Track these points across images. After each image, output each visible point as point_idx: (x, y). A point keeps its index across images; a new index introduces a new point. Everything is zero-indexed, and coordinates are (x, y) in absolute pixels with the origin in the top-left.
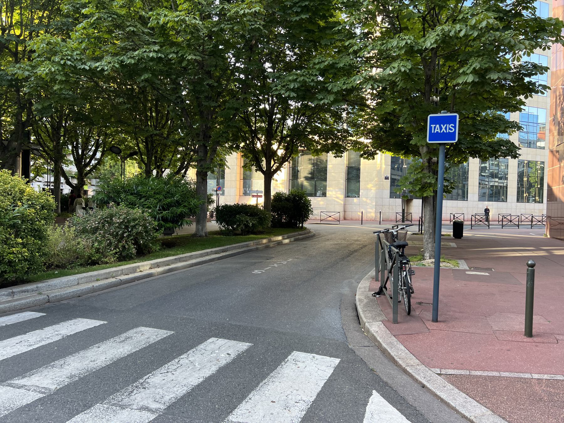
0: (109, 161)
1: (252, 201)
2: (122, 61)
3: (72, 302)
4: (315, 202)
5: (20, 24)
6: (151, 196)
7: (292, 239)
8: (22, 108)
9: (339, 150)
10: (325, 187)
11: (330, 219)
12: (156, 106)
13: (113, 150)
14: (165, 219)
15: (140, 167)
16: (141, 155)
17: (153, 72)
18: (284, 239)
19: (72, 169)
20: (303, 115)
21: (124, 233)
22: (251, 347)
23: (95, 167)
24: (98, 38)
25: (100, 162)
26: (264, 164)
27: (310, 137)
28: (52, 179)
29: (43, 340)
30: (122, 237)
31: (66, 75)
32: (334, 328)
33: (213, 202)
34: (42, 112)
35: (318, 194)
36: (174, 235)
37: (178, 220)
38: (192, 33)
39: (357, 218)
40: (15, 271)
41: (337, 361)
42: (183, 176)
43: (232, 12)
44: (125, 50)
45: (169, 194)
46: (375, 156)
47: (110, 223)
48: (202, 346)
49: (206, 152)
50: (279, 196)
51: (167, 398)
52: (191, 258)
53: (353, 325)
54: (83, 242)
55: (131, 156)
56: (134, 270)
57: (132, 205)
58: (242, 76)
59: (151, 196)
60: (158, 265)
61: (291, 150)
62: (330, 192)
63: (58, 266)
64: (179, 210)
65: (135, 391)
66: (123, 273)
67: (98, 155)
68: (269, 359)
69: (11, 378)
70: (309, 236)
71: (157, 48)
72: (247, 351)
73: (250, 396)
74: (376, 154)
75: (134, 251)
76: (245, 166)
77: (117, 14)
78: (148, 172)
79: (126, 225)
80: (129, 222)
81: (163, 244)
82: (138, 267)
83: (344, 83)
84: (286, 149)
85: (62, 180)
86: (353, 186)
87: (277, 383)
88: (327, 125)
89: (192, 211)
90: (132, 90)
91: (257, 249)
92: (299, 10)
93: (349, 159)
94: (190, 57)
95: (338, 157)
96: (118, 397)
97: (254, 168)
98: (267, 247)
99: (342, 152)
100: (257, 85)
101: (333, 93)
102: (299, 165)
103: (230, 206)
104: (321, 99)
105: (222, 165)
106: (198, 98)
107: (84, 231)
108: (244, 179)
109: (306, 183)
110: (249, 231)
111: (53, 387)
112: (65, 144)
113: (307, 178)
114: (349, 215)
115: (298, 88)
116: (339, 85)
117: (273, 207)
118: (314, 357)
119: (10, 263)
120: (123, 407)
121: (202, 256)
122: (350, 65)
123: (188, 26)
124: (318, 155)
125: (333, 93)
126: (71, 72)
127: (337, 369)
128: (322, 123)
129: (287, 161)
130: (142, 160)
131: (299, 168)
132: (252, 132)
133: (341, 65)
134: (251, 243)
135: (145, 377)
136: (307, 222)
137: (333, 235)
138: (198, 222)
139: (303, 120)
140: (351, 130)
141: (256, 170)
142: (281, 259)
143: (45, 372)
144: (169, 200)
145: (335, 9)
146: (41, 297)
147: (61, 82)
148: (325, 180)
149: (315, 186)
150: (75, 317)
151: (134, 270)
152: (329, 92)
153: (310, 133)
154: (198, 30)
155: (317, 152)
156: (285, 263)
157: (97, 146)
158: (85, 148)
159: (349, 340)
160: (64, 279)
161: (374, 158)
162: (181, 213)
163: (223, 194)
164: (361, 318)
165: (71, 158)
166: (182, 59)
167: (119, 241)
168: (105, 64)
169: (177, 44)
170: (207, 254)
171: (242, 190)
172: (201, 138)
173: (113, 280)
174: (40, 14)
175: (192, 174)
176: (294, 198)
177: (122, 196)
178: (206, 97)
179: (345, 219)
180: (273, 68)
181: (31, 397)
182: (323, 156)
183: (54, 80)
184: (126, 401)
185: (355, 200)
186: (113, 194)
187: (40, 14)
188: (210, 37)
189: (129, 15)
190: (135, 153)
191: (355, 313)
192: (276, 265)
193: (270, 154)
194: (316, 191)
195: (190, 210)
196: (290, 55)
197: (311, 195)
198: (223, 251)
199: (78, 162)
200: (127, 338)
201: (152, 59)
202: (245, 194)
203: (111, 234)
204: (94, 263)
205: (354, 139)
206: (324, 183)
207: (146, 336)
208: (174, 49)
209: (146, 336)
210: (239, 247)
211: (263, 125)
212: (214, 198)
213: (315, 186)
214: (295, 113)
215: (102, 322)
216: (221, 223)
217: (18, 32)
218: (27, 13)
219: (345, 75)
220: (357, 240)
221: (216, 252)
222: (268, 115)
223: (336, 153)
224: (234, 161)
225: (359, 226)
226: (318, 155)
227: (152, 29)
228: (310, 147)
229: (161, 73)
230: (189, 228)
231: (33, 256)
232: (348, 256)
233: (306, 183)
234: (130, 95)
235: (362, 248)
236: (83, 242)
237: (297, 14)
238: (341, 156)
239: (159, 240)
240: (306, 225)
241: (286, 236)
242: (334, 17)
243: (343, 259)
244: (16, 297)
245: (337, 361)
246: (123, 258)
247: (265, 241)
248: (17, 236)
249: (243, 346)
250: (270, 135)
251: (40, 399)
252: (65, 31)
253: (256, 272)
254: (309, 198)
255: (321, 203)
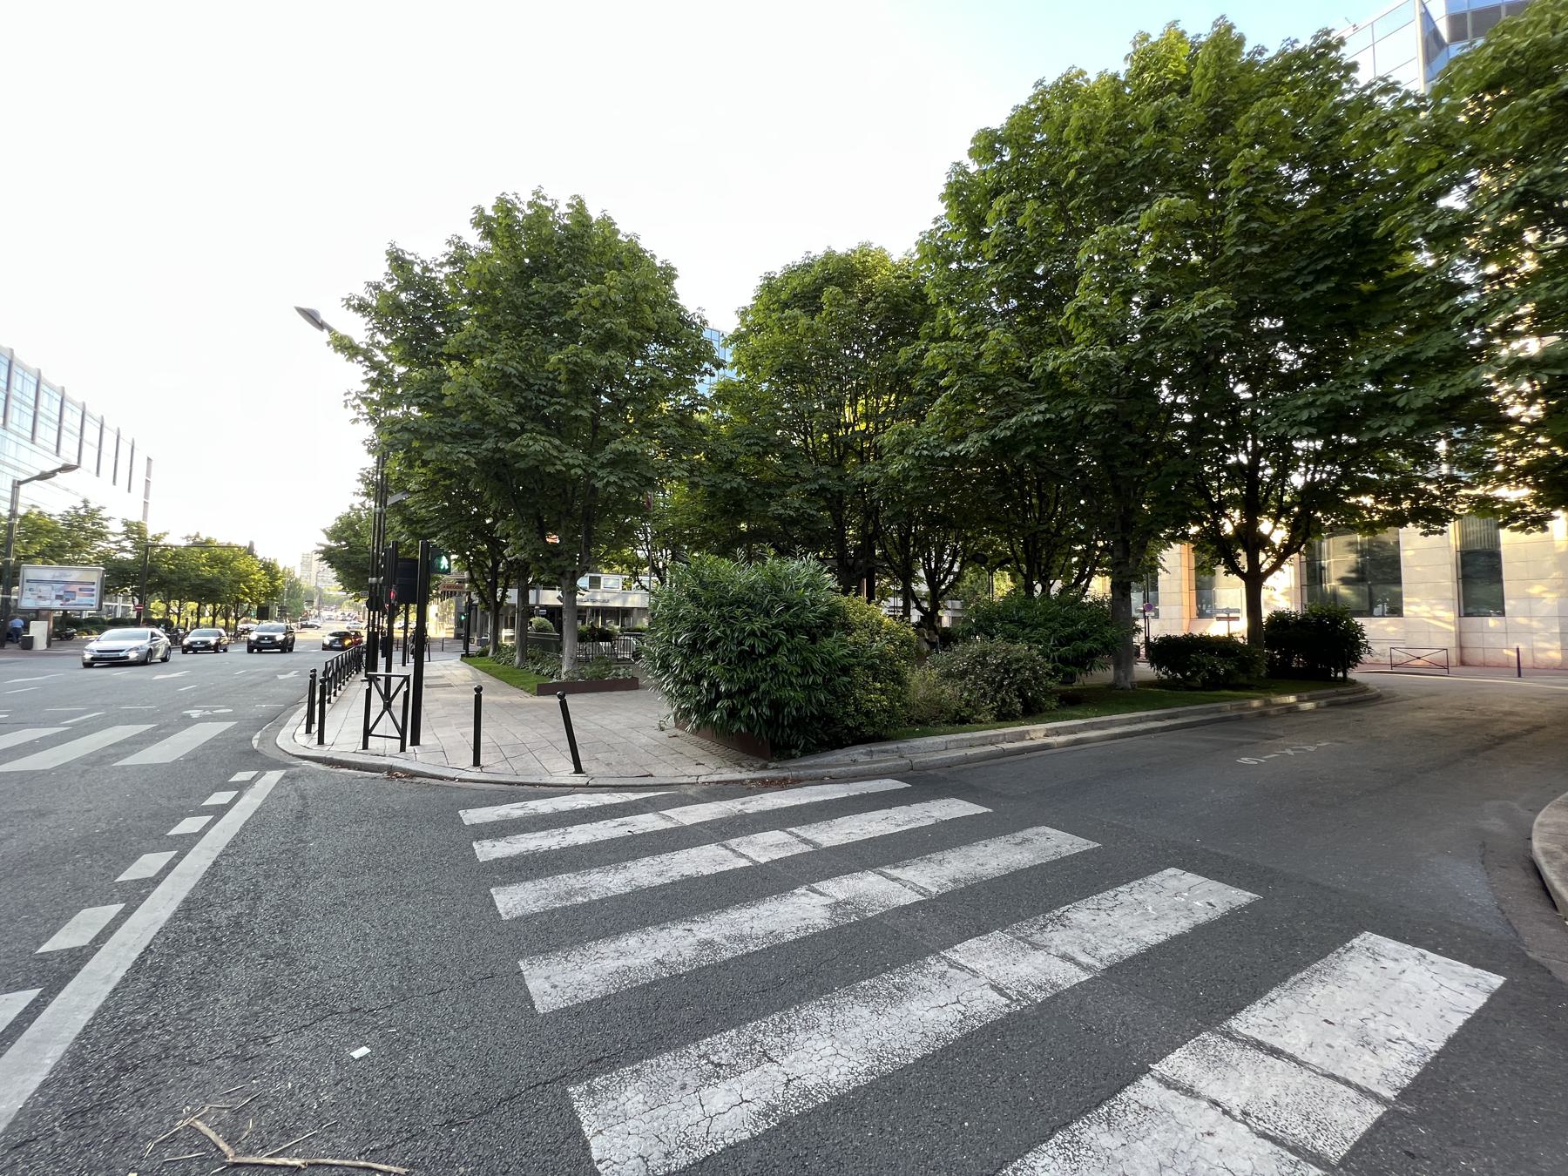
0: (969, 574)
1: (1215, 629)
2: (993, 437)
3: (941, 774)
4: (1376, 629)
5: (866, 417)
6: (1040, 625)
7: (1323, 703)
8: (868, 517)
9: (1432, 516)
10: (1399, 596)
11: (1419, 662)
12: (1039, 489)
13: (976, 559)
14: (1062, 660)
15: (1013, 580)
16: (1018, 562)
17: (1038, 441)
18: (1300, 701)
19: (923, 588)
20: (1332, 462)
21: (1003, 679)
22: (1257, 901)
23: (952, 585)
24: (961, 413)
25: (959, 577)
26: (1243, 561)
27: (1353, 500)
28: (901, 604)
29: (910, 822)
30: (1001, 686)
31: (922, 469)
32: (1472, 904)
33: (1139, 630)
34: (890, 520)
35: (1377, 611)
36: (1076, 685)
37: (1084, 661)
38: (1098, 372)
39: (1503, 661)
40: (873, 725)
41: (1497, 981)
42: (1085, 590)
43: (1170, 321)
44: (996, 420)
45: (1069, 621)
46: (1549, 524)
47: (984, 665)
48: (1154, 879)
49: (1127, 552)
50: (1280, 619)
51: (1105, 952)
52: (1111, 724)
53: (1536, 907)
54: (949, 690)
55: (1001, 565)
56: (1021, 736)
57: (1013, 638)
58: (1188, 418)
59: (1040, 625)
60: (1057, 732)
61: (1304, 534)
62: (1413, 607)
63: (918, 722)
64: (1087, 646)
65: (1050, 927)
66: (1005, 738)
67: (956, 569)
68: (1305, 934)
69: (882, 865)
70: (1365, 698)
71: (1043, 407)
72: (1249, 906)
73: (1273, 994)
74: (1552, 518)
75: (1019, 707)
76: (1200, 568)
77: (984, 375)
78: (1030, 588)
79: (1006, 667)
80: (1010, 663)
81: (1061, 699)
82: (1028, 732)
83: (1442, 388)
84: (1294, 528)
85: (913, 605)
86: (1480, 591)
87: (1332, 988)
88: (1393, 473)
89: (1108, 647)
90: (1003, 471)
91: (1240, 718)
92: (1310, 279)
93: (1464, 536)
94: (1096, 409)
95: (1435, 533)
96: (1026, 928)
97: (1221, 569)
98: (1263, 715)
99: (1443, 522)
100: (1219, 427)
101: (1412, 411)
102: (1325, 555)
103: (1176, 639)
104: (1381, 428)
105: (1153, 568)
106: (1110, 467)
107: (949, 675)
108: (1197, 588)
109: (1344, 591)
110: (1216, 683)
111: (934, 890)
112: (916, 556)
113: (1345, 581)
114: (1475, 655)
115: (1320, 416)
116: (1433, 390)
117: (1268, 638)
118: (1424, 956)
119: (868, 713)
120: (1036, 947)
121: (1130, 722)
122: (1455, 348)
123: (1091, 363)
124: (1374, 533)
125: (1412, 411)
126: (928, 464)
127: (1495, 997)
128: (1379, 472)
129: (1297, 550)
130: (1019, 570)
131: (1324, 563)
132: (1212, 506)
133: (1431, 353)
134: (1227, 705)
135: (1063, 909)
136: (1356, 670)
137: (1434, 699)
138: (1117, 666)
139: (1330, 473)
140: (1465, 476)
141: (1227, 573)
142: (1295, 742)
143: (921, 866)
144: (1069, 630)
145: (1399, 252)
146: (903, 762)
147: (916, 479)
148: (1398, 581)
149: (1371, 594)
150: (948, 797)
151: (1021, 736)
152: (1404, 411)
153: (1348, 494)
154: (1109, 365)
155: (1371, 527)
156: (1312, 749)
157: (954, 554)
158: (939, 560)
159: (1527, 939)
160: (930, 740)
161: (1545, 529)
162: (1090, 650)
163: (1157, 616)
164: (1559, 896)
165: (921, 573)
166: (1085, 413)
167: (997, 692)
168: (969, 446)
169: (1075, 394)
170: (1141, 720)
171: (1194, 609)
172: (1117, 527)
173: (993, 748)
174: (886, 398)
175: (1100, 587)
176: (1319, 621)
177: (998, 624)
178: (1124, 464)
179: (1463, 663)
180: (1252, 390)
181: (908, 898)
182: (1387, 536)
183: (906, 479)
184: (1037, 937)
185: (1492, 622)
186: (988, 621)
187: (886, 398)
188: (1127, 369)
189: (1001, 371)
190: (1008, 560)
191: (1533, 880)
192: (1289, 752)
193: (1255, 543)
194: (1372, 605)
195: (1106, 645)
196: (1288, 358)
197: (1360, 614)
198: (1170, 717)
199: (931, 577)
200: (1025, 840)
201: (1037, 424)
202: (1201, 614)
203: (986, 681)
204: (963, 721)
205: (1479, 491)
206: (1396, 589)
207: (1049, 843)
208: (1071, 402)
209: (1049, 843)
210: (1201, 712)
211: (1237, 491)
212: (1141, 623)
213: (1371, 594)
214: (1307, 462)
215: (981, 810)
216: (1159, 668)
217: (863, 426)
218: (873, 401)
219: (1440, 371)
220: (1511, 713)
221: (1157, 719)
222: (1247, 474)
223: (1424, 527)
224: (1175, 562)
225: (1515, 682)
226: (1374, 533)
227: (1036, 381)
228: (1352, 520)
229: (1049, 441)
230: (1104, 675)
231: (893, 707)
232: (1489, 748)
233: (1344, 591)
234: (1002, 479)
235: (1529, 732)
236: (949, 690)
237: (1305, 287)
238: (1442, 532)
239: (1055, 692)
240: (1353, 674)
241: (1305, 696)
242: (1398, 266)
243: (1473, 753)
244: (875, 758)
245: (1497, 981)
246: (1004, 716)
247: (1256, 703)
248: (875, 680)
249: (1242, 897)
250: (1253, 507)
251: (919, 903)
252: (917, 414)
253: (1245, 760)
254: (1359, 620)
255: (1391, 629)
